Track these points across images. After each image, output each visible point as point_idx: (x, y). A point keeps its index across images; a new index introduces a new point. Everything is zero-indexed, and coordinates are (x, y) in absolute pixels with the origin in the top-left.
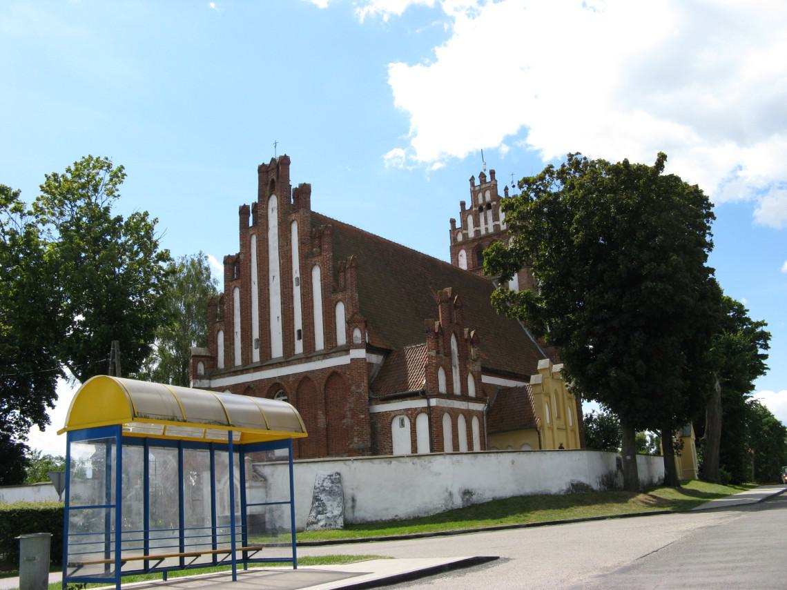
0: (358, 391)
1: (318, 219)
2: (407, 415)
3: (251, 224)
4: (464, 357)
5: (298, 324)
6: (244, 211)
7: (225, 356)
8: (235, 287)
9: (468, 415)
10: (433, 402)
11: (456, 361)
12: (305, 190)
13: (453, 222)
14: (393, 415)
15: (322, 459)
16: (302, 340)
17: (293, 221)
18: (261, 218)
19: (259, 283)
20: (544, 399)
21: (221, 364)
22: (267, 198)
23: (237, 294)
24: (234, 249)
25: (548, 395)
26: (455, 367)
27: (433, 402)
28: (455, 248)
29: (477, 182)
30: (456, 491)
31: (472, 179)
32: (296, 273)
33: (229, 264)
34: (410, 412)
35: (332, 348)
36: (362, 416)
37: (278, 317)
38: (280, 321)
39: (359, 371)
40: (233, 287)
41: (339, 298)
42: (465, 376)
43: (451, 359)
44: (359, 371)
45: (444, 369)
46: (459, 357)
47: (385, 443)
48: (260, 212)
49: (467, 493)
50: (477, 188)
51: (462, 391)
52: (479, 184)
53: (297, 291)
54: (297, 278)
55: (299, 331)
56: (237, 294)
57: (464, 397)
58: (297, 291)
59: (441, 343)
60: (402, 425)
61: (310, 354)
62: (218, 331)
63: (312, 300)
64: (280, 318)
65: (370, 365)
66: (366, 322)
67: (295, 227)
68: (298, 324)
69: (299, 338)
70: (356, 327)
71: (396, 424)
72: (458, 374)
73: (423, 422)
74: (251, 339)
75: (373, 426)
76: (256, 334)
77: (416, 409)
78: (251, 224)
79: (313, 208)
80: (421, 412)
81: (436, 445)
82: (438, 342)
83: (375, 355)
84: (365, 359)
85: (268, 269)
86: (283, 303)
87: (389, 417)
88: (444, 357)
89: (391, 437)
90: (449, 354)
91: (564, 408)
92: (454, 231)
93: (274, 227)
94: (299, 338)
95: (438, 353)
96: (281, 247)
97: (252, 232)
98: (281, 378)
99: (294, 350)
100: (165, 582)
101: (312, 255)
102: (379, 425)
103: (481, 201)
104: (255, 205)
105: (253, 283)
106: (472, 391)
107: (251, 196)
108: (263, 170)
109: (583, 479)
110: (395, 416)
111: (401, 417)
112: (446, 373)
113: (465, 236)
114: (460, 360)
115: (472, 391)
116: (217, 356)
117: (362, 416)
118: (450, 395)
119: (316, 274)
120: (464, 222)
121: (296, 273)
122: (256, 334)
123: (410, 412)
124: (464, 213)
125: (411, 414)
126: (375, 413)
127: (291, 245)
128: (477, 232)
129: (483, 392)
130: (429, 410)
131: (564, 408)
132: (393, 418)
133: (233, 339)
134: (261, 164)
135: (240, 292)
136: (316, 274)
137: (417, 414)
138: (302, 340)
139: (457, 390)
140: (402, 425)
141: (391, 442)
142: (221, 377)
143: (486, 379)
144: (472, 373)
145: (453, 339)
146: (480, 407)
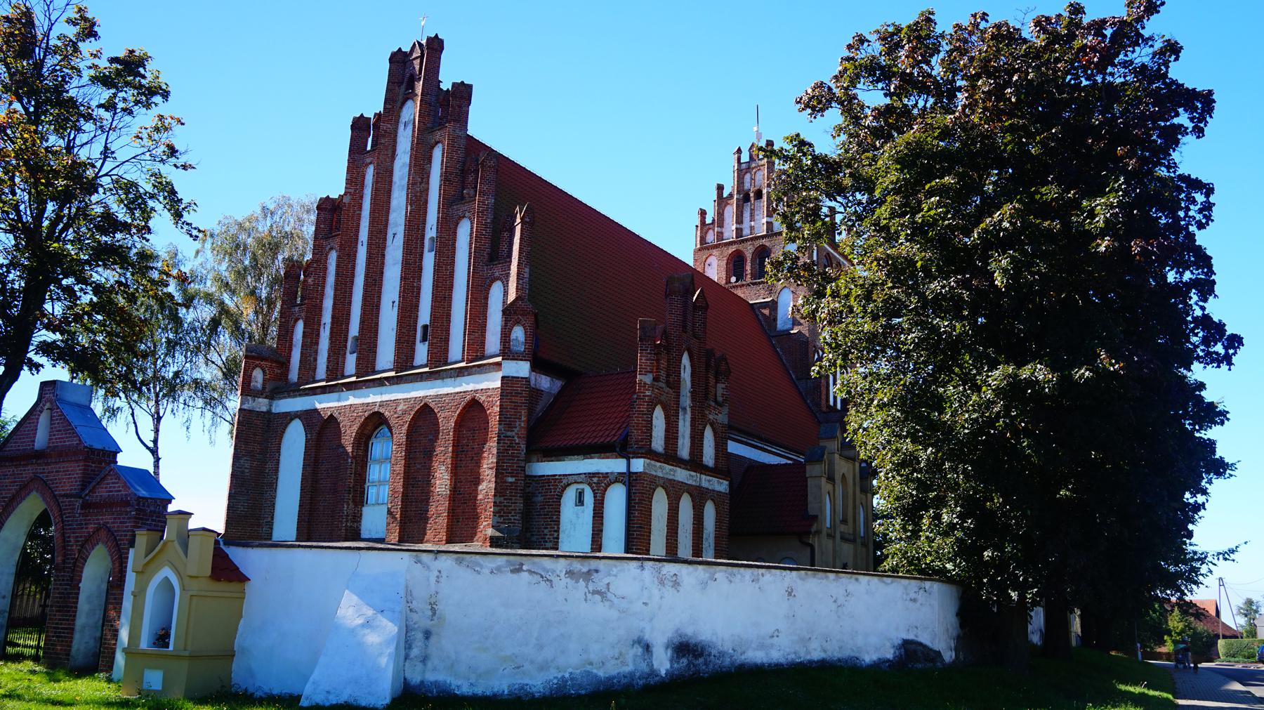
0: (509, 434)
1: (475, 147)
2: (590, 484)
3: (369, 148)
4: (701, 395)
5: (424, 317)
6: (360, 125)
7: (301, 361)
8: (332, 249)
9: (699, 497)
10: (638, 465)
11: (686, 401)
12: (463, 92)
13: (703, 213)
14: (565, 481)
15: (509, 551)
16: (427, 343)
17: (437, 143)
18: (384, 136)
19: (370, 245)
20: (826, 486)
21: (294, 375)
22: (399, 104)
23: (333, 258)
24: (336, 188)
25: (831, 479)
26: (685, 409)
27: (638, 465)
28: (704, 247)
29: (745, 158)
30: (660, 639)
31: (739, 151)
32: (431, 232)
33: (325, 209)
34: (595, 480)
35: (600, 483)
36: (510, 480)
37: (393, 302)
38: (396, 309)
39: (514, 399)
40: (327, 249)
41: (497, 274)
42: (700, 427)
43: (678, 395)
44: (514, 399)
45: (664, 408)
46: (694, 394)
47: (546, 531)
48: (383, 126)
49: (684, 648)
50: (744, 166)
51: (691, 453)
52: (748, 160)
53: (429, 260)
54: (432, 239)
55: (425, 327)
56: (333, 258)
57: (695, 463)
58: (429, 260)
59: (663, 364)
60: (580, 501)
61: (439, 367)
62: (297, 320)
63: (452, 275)
64: (397, 304)
65: (535, 393)
66: (536, 315)
67: (437, 154)
68: (424, 317)
69: (424, 339)
70: (518, 322)
71: (569, 496)
72: (688, 424)
73: (616, 498)
74: (346, 336)
75: (528, 499)
76: (354, 329)
77: (606, 475)
78: (369, 148)
79: (471, 131)
80: (616, 481)
81: (636, 542)
82: (658, 361)
83: (549, 379)
84: (527, 380)
85: (387, 220)
86: (403, 278)
87: (557, 485)
88: (667, 389)
89: (558, 522)
90: (675, 385)
91: (855, 507)
92: (704, 227)
93: (404, 152)
94: (424, 339)
95: (656, 379)
96: (412, 185)
97: (368, 160)
98: (382, 404)
99: (413, 358)
100: (838, 521)
101: (461, 198)
102: (540, 499)
103: (747, 186)
104: (378, 116)
105: (360, 244)
106: (709, 456)
107: (373, 105)
108: (399, 60)
109: (925, 639)
110: (569, 485)
111: (581, 486)
112: (667, 417)
113: (720, 236)
114: (693, 399)
115: (709, 456)
116: (289, 362)
117: (510, 480)
118: (670, 456)
119: (464, 232)
120: (720, 214)
121: (431, 232)
122: (354, 329)
123: (595, 480)
124: (722, 201)
125: (598, 483)
126: (535, 476)
127: (428, 183)
128: (739, 232)
129: (726, 466)
130: (629, 479)
131: (855, 507)
132: (564, 488)
133: (318, 335)
134: (396, 50)
135: (339, 257)
136: (464, 232)
137: (608, 485)
138: (427, 343)
139: (684, 451)
140: (580, 501)
141: (558, 531)
142: (289, 396)
143: (733, 448)
144: (712, 425)
145: (686, 360)
146: (722, 486)
